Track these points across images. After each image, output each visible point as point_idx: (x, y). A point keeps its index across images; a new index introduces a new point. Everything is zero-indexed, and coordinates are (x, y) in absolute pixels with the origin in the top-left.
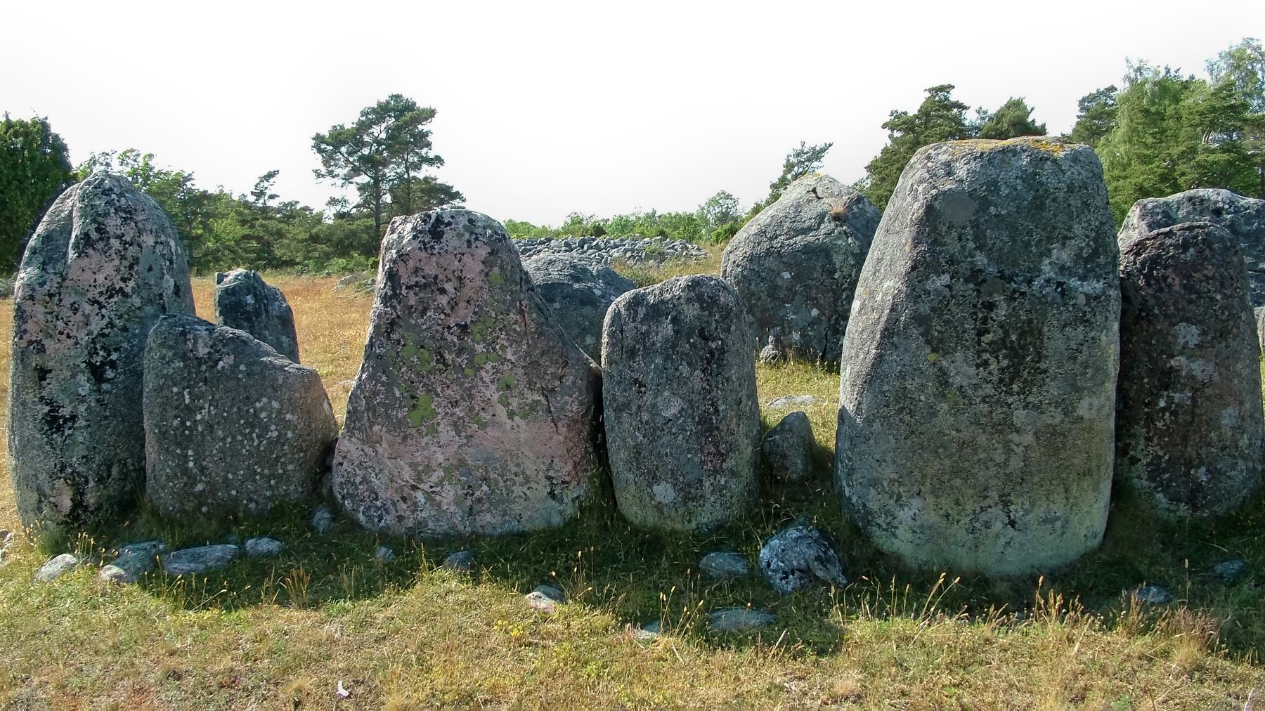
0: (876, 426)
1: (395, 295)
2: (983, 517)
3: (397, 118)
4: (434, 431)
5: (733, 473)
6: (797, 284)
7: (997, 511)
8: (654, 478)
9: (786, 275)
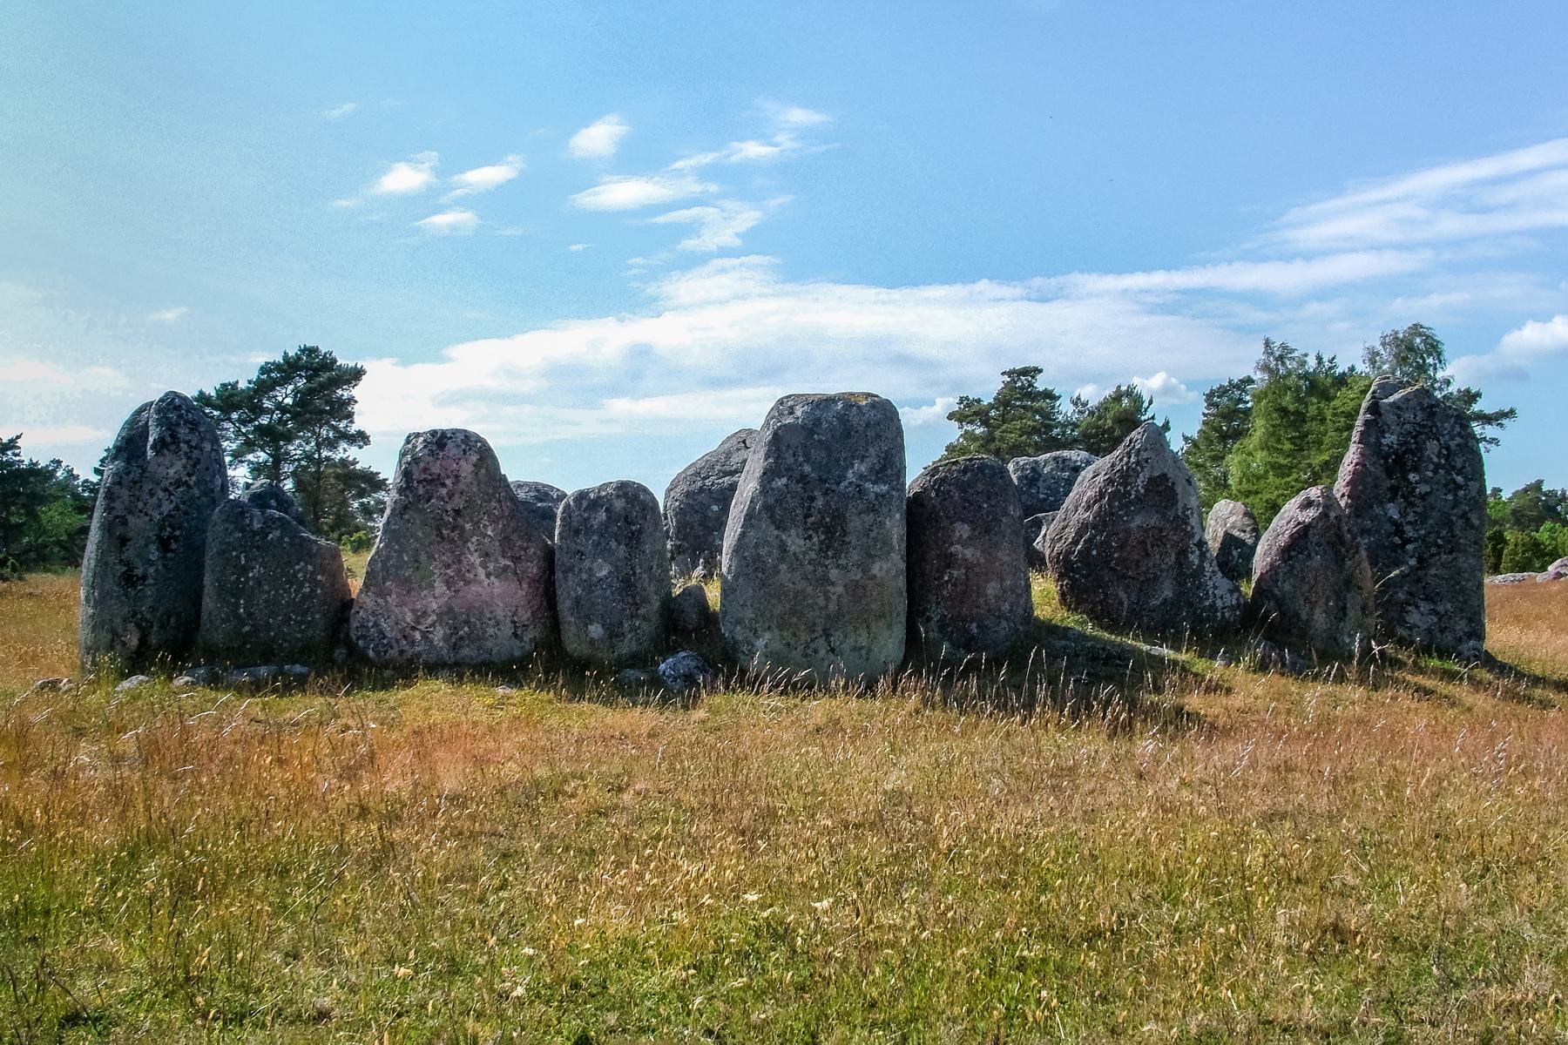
0: (741, 580)
1: (408, 487)
2: (812, 646)
3: (309, 379)
4: (431, 586)
5: (644, 618)
6: (704, 502)
7: (822, 641)
8: (588, 620)
9: (715, 508)
